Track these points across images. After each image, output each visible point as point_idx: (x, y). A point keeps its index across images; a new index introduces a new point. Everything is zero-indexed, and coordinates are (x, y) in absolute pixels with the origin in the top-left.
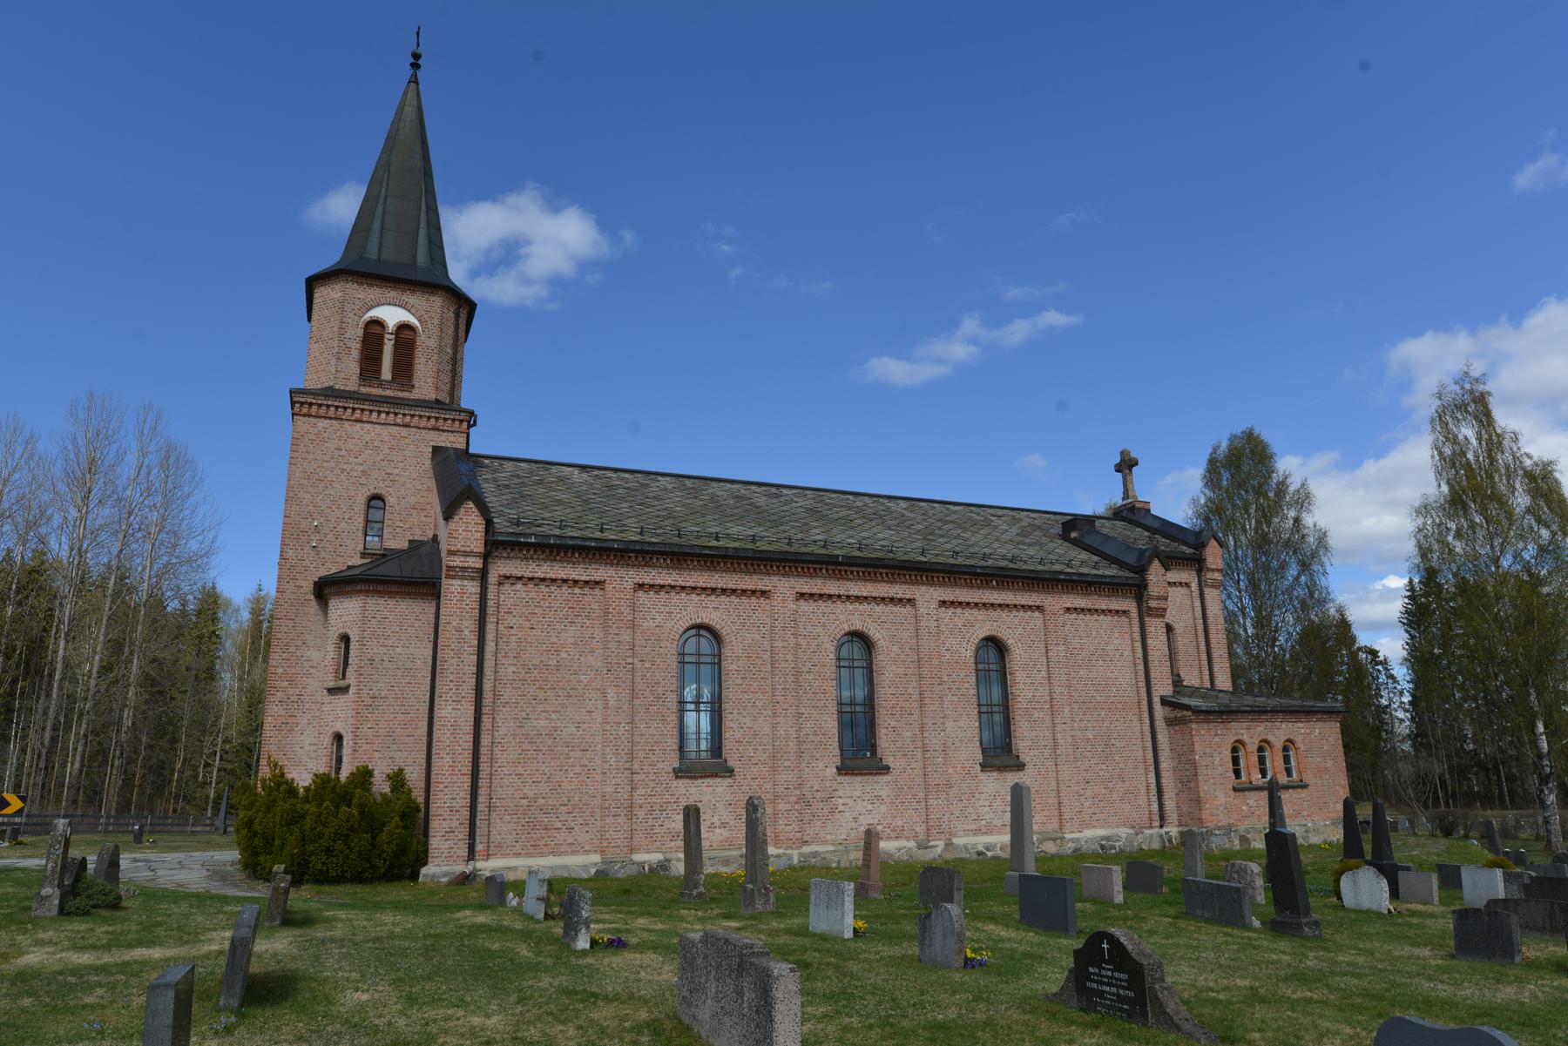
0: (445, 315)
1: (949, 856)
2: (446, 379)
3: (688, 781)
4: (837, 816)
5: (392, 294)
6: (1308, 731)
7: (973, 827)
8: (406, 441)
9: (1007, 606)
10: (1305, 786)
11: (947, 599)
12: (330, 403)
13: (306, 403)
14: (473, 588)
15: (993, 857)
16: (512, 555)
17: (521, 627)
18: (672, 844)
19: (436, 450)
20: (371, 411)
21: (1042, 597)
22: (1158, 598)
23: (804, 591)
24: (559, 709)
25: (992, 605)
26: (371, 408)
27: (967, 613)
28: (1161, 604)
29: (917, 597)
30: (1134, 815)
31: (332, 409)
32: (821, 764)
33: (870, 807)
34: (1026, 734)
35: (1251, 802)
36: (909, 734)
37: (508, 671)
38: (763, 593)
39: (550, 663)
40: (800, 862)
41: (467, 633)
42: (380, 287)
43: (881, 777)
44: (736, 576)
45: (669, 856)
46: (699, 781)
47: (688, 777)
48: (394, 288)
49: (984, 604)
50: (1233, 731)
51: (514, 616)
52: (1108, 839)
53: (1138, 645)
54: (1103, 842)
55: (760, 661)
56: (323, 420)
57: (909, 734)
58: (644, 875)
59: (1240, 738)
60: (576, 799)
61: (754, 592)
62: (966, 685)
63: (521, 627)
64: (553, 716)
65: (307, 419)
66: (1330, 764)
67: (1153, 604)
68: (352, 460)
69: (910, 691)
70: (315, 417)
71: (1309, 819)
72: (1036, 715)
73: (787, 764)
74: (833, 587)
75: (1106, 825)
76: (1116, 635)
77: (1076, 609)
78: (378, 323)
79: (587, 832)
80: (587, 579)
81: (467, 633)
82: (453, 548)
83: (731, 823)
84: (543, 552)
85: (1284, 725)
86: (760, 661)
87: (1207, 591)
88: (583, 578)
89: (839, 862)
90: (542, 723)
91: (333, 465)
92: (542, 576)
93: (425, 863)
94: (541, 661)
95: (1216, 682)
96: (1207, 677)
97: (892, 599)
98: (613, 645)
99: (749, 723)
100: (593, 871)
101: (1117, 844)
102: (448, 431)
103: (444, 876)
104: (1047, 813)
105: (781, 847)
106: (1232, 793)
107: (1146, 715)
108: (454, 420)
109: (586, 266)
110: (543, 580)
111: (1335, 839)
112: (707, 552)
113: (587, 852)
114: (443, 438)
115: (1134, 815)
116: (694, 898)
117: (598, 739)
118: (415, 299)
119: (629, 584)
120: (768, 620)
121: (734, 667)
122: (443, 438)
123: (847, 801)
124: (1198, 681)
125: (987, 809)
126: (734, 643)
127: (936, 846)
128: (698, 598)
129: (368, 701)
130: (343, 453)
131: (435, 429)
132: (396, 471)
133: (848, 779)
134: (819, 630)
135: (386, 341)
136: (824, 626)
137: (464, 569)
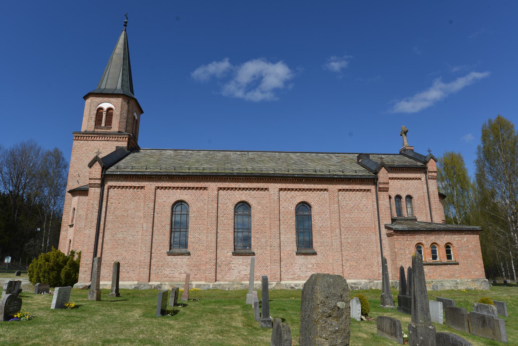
1: (277, 288)
3: (172, 256)
4: (231, 271)
6: (460, 239)
7: (292, 277)
8: (108, 145)
10: (458, 264)
11: (283, 188)
12: (84, 135)
13: (77, 136)
14: (98, 190)
15: (298, 289)
17: (115, 203)
18: (165, 279)
20: (97, 137)
22: (384, 183)
23: (221, 187)
24: (126, 231)
26: (97, 136)
27: (293, 193)
28: (386, 186)
30: (371, 274)
31: (85, 137)
32: (225, 251)
33: (245, 268)
34: (318, 240)
36: (264, 240)
37: (109, 218)
39: (125, 215)
40: (213, 287)
42: (102, 97)
45: (162, 283)
46: (177, 256)
47: (172, 255)
50: (417, 239)
51: (113, 199)
52: (355, 284)
53: (375, 203)
54: (352, 285)
55: (203, 213)
57: (264, 240)
58: (152, 289)
59: (421, 242)
60: (131, 262)
62: (291, 221)
63: (115, 203)
64: (125, 233)
66: (472, 254)
67: (381, 186)
69: (265, 223)
70: (80, 140)
71: (459, 278)
72: (323, 233)
73: (210, 251)
75: (356, 278)
76: (364, 200)
78: (101, 109)
79: (134, 273)
80: (138, 186)
81: (95, 205)
82: (90, 177)
84: (123, 177)
86: (203, 213)
87: (429, 181)
88: (137, 186)
89: (229, 288)
90: (120, 235)
91: (84, 155)
92: (123, 185)
94: (122, 214)
95: (433, 219)
96: (429, 217)
98: (146, 208)
99: (197, 235)
100: (133, 287)
101: (359, 286)
102: (121, 141)
103: (81, 286)
105: (206, 282)
107: (378, 233)
108: (123, 137)
109: (286, 82)
111: (473, 288)
113: (134, 280)
115: (371, 274)
116: (110, 296)
117: (140, 241)
118: (112, 100)
119: (153, 187)
120: (207, 198)
121: (192, 215)
122: (120, 143)
123: (236, 265)
124: (425, 219)
125: (298, 270)
126: (193, 207)
128: (180, 191)
129: (78, 229)
130: (88, 151)
133: (237, 257)
135: (103, 114)
136: (230, 199)
137: (94, 184)
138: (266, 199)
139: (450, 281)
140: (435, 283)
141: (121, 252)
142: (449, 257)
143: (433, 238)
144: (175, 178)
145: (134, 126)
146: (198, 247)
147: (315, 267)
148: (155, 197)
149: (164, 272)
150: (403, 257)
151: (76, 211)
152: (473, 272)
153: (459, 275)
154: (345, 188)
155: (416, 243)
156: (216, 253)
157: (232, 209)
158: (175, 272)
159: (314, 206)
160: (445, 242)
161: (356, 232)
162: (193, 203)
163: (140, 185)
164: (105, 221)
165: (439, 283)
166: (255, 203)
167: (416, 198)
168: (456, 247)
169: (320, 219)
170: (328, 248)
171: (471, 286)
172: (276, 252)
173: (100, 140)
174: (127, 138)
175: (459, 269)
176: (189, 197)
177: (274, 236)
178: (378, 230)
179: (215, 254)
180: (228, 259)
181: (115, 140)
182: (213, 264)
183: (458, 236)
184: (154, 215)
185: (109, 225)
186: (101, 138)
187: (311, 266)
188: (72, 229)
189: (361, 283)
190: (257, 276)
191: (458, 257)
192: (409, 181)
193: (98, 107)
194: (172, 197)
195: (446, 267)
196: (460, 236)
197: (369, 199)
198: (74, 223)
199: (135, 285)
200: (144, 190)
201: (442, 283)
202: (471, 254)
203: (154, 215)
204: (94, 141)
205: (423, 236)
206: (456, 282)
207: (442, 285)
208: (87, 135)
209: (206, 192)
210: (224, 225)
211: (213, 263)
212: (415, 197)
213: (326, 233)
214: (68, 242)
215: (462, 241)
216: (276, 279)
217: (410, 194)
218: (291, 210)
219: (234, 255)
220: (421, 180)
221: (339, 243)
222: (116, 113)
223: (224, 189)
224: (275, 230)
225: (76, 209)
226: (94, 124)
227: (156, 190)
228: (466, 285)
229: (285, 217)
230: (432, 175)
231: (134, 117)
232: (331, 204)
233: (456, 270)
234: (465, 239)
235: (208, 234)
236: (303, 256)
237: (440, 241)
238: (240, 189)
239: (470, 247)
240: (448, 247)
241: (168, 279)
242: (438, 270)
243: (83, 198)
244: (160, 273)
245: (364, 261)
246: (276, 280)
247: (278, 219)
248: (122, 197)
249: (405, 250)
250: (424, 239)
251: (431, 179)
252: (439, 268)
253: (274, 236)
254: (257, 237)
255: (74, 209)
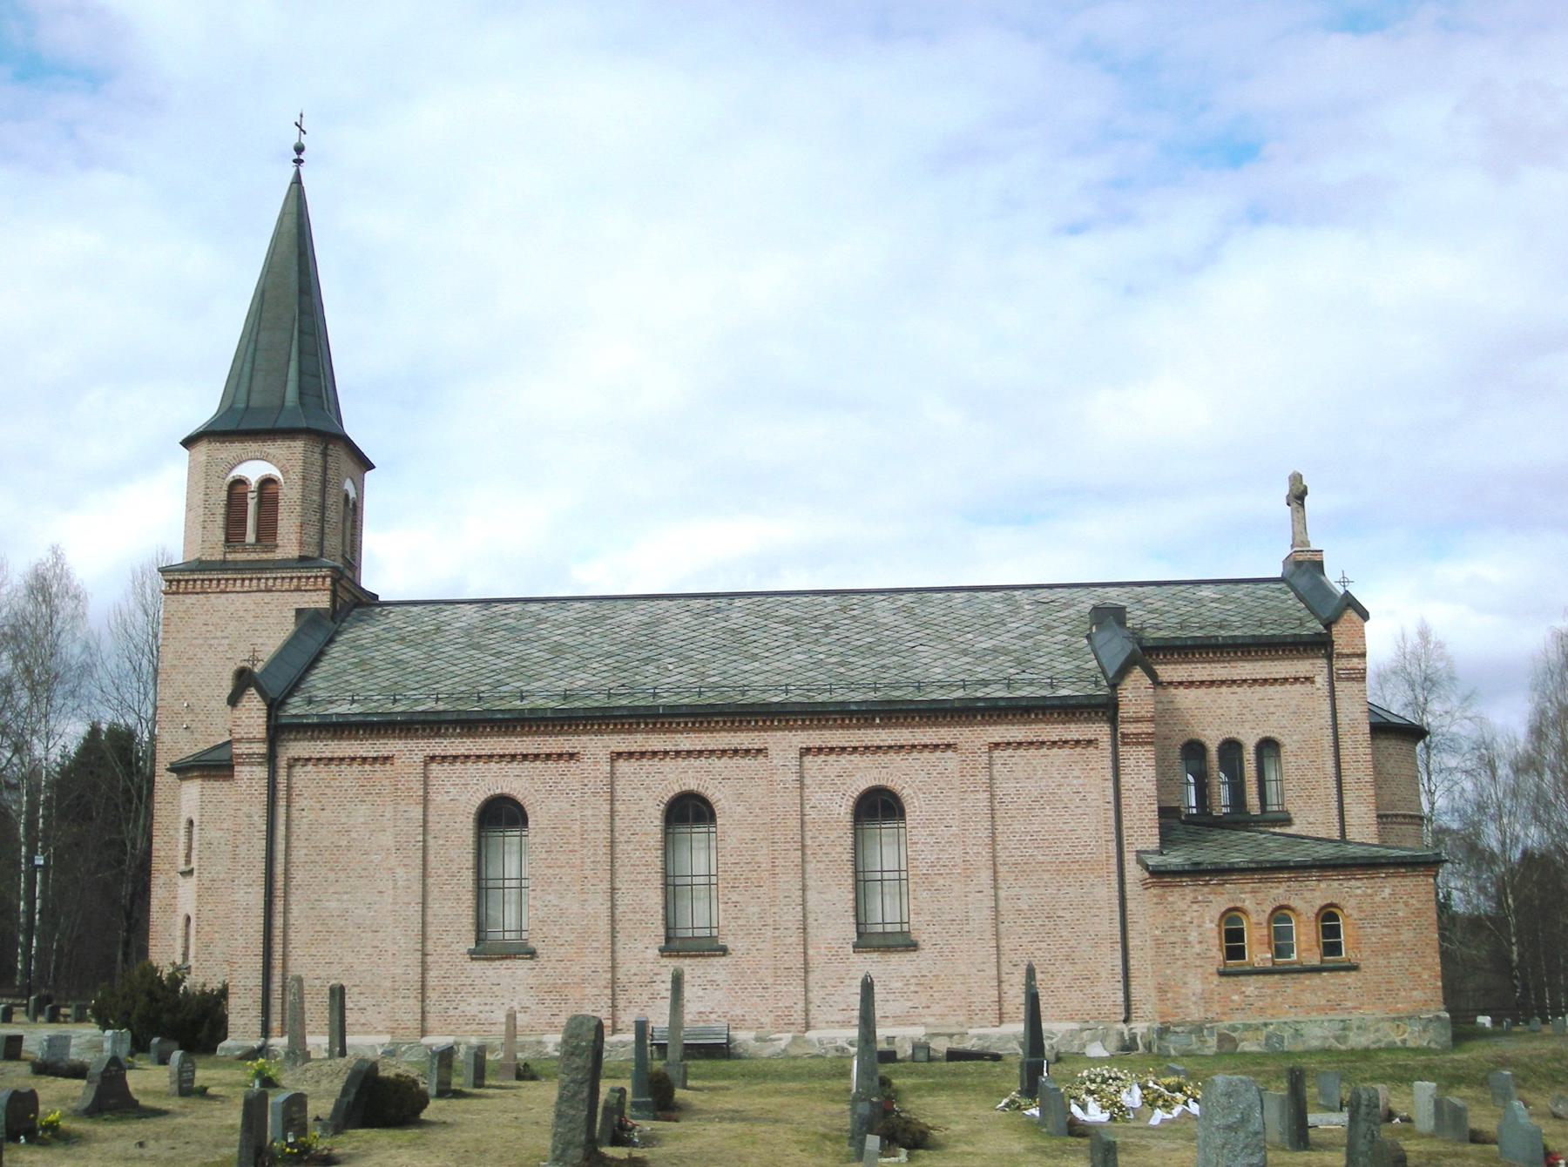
0: (308, 460)
1: (794, 1051)
2: (313, 531)
5: (253, 447)
6: (1369, 891)
7: (839, 1017)
8: (270, 607)
9: (902, 747)
12: (196, 577)
13: (174, 580)
14: (261, 772)
16: (298, 737)
18: (468, 1027)
19: (299, 612)
20: (235, 580)
21: (956, 731)
25: (879, 748)
26: (235, 576)
27: (844, 759)
29: (770, 746)
30: (1088, 1006)
32: (640, 946)
35: (1250, 990)
37: (299, 855)
38: (572, 756)
41: (256, 818)
43: (717, 959)
44: (504, 740)
46: (497, 963)
48: (255, 441)
49: (867, 748)
53: (1110, 784)
55: (569, 832)
56: (190, 596)
57: (756, 909)
59: (1239, 905)
61: (560, 756)
62: (839, 849)
65: (177, 596)
68: (219, 634)
69: (757, 859)
72: (941, 882)
73: (595, 945)
74: (657, 742)
76: (1076, 773)
77: (1009, 744)
78: (240, 482)
80: (375, 755)
83: (533, 1007)
84: (328, 731)
85: (1323, 885)
92: (330, 755)
93: (225, 1037)
97: (736, 751)
102: (310, 591)
103: (239, 1050)
104: (949, 1003)
106: (1216, 979)
107: (1114, 877)
110: (331, 759)
111: (1398, 1040)
112: (499, 716)
113: (380, 1032)
114: (306, 599)
115: (1088, 1006)
119: (419, 758)
120: (578, 786)
121: (538, 840)
127: (780, 1039)
128: (498, 765)
129: (207, 884)
130: (211, 628)
131: (298, 590)
132: (260, 641)
134: (643, 793)
135: (249, 501)
136: (648, 788)
138: (760, 782)
139: (1323, 1022)
140: (1275, 1029)
141: (339, 952)
142: (1332, 948)
143: (1281, 891)
144: (481, 729)
145: (348, 524)
146: (557, 934)
147: (913, 988)
148: (425, 789)
149: (463, 1006)
150: (1178, 951)
151: (196, 830)
152: (1404, 993)
153: (1356, 1004)
154: (1011, 740)
155: (1223, 909)
156: (613, 952)
157: (657, 818)
158: (493, 1008)
159: (912, 798)
160: (1319, 903)
161: (1046, 876)
162: (537, 801)
163: (380, 754)
164: (287, 862)
165: (1287, 1028)
166: (725, 797)
167: (1294, 747)
168: (1356, 917)
169: (932, 840)
170: (954, 928)
171: (1392, 1034)
172: (791, 944)
173: (245, 589)
174: (328, 581)
175: (1359, 984)
176: (527, 785)
177: (786, 897)
178: (1114, 868)
179: (608, 953)
180: (649, 967)
181: (292, 588)
182: (604, 983)
183: (1365, 881)
184: (425, 841)
185: (299, 876)
186: (247, 582)
187: (899, 985)
188: (193, 880)
189: (1052, 1033)
190: (737, 1016)
191: (1357, 948)
192: (1271, 690)
193: (230, 478)
194: (476, 787)
195: (1316, 980)
196: (1373, 881)
197: (1092, 769)
198: (194, 864)
199: (383, 1045)
200: (393, 768)
201: (1299, 1027)
202: (1402, 938)
203: (425, 841)
204: (225, 595)
205: (1248, 888)
206: (1342, 1024)
207: (1297, 1034)
208: (205, 577)
209: (578, 767)
210: (632, 865)
211: (605, 979)
212: (1289, 744)
213: (948, 882)
214: (181, 922)
215: (1377, 899)
216: (793, 1024)
217: (1273, 735)
218: (839, 814)
219: (666, 956)
220: (1313, 682)
221: (988, 913)
222: (290, 497)
223: (631, 754)
224: (790, 882)
225: (196, 823)
226: (223, 538)
227: (426, 764)
228: (1377, 1030)
229: (821, 838)
230: (1349, 666)
231: (347, 496)
232: (966, 791)
233: (1350, 988)
234: (1387, 891)
235: (585, 896)
236: (875, 956)
237: (1302, 899)
238: (678, 753)
239: (1400, 914)
240: (1329, 919)
241: (475, 1027)
242: (1288, 990)
243: (217, 788)
244: (451, 1012)
245: (1068, 967)
246: (792, 1028)
247: (796, 846)
248: (328, 791)
249: (1185, 931)
250: (1248, 895)
251: (1348, 679)
252: (1291, 985)
253: (786, 897)
254: (734, 900)
255: (191, 823)
